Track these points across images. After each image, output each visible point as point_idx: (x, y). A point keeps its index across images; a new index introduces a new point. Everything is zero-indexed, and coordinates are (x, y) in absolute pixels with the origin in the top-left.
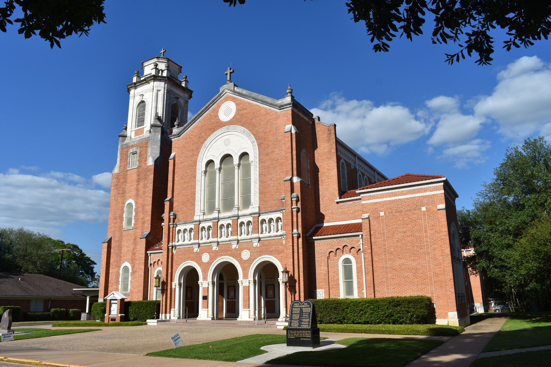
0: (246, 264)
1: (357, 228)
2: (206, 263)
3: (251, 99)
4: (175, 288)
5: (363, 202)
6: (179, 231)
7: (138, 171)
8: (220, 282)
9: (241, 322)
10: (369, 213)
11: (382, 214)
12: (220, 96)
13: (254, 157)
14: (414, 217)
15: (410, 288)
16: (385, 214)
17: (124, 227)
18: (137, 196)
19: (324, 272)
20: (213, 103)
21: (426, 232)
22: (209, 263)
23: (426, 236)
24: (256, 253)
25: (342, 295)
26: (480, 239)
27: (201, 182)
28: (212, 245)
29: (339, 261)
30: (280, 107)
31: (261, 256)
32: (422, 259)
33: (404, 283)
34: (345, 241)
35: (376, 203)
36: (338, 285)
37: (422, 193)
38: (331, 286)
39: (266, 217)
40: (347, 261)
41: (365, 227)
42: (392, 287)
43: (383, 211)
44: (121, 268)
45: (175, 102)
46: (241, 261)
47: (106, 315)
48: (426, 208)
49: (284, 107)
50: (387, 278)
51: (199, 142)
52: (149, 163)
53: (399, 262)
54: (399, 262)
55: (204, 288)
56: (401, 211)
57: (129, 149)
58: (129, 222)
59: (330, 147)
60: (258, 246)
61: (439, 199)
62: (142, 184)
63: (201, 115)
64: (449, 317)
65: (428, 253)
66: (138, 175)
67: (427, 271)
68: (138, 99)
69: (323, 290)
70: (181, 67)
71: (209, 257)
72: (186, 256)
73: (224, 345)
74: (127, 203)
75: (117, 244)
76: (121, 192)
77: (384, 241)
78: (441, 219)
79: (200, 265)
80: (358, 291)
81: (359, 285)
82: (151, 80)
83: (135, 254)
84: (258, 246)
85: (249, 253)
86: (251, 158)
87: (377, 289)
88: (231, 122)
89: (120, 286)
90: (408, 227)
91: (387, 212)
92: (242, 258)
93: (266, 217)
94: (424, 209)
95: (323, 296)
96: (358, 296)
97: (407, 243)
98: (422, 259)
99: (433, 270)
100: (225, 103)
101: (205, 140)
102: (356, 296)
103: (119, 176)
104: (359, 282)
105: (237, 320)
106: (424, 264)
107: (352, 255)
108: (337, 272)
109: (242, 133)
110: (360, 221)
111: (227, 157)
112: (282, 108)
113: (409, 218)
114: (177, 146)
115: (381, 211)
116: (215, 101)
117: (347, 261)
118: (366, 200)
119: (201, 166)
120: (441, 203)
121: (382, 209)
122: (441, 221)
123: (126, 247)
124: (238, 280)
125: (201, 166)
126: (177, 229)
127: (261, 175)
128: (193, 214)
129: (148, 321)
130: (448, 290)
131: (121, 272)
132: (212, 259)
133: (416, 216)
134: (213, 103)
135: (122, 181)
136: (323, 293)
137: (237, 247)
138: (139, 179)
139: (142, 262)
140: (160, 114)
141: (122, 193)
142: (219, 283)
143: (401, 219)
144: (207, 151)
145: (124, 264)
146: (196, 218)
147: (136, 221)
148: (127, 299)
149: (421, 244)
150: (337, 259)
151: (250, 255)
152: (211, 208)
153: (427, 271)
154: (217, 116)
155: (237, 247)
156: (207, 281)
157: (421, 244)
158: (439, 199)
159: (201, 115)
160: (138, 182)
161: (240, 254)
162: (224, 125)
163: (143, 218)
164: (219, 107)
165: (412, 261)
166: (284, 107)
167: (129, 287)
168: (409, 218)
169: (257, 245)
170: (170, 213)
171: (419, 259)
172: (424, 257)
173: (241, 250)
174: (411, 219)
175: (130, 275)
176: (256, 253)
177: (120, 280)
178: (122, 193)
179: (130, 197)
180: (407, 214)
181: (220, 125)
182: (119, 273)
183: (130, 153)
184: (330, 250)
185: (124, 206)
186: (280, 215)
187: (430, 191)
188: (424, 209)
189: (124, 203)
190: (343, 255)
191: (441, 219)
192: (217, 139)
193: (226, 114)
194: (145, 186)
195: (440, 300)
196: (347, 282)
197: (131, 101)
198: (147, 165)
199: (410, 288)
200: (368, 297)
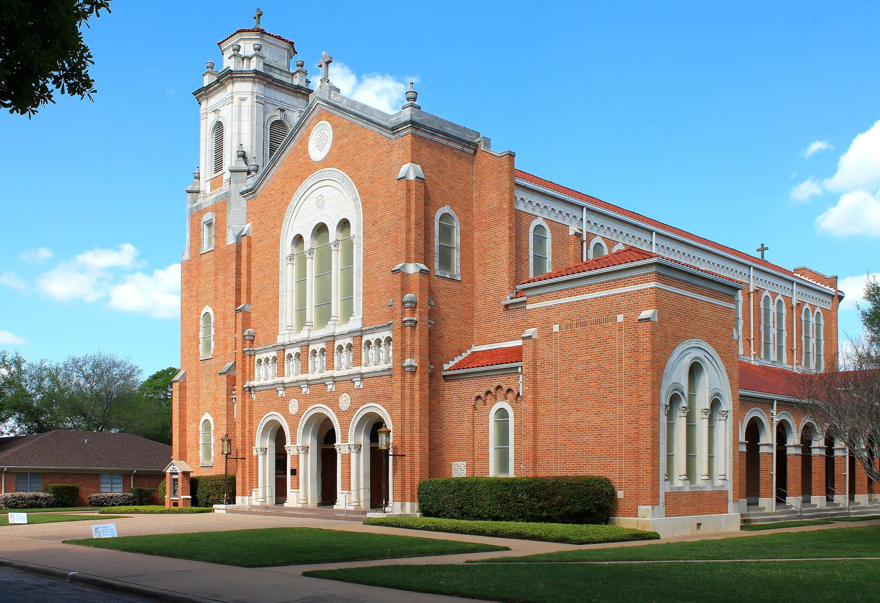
0: (293, 420)
1: (516, 354)
2: (294, 415)
3: (352, 116)
4: (257, 456)
5: (529, 307)
6: (260, 361)
7: (215, 256)
8: (323, 447)
9: (338, 511)
10: (536, 327)
11: (556, 328)
12: (309, 113)
13: (356, 230)
14: (605, 334)
15: (589, 462)
16: (560, 328)
17: (201, 355)
18: (215, 302)
19: (466, 432)
20: (300, 126)
21: (620, 361)
22: (298, 415)
23: (620, 369)
24: (359, 399)
25: (493, 472)
26: (85, 426)
27: (288, 274)
28: (301, 386)
29: (491, 410)
30: (392, 131)
31: (365, 404)
32: (610, 411)
33: (581, 453)
34: (501, 381)
35: (548, 309)
36: (487, 454)
37: (585, 295)
38: (477, 457)
39: (372, 337)
40: (502, 413)
41: (527, 353)
42: (562, 460)
43: (557, 324)
44: (201, 423)
45: (278, 118)
46: (287, 416)
47: (166, 497)
48: (624, 317)
49: (399, 130)
50: (556, 444)
51: (283, 203)
52: (229, 242)
53: (575, 416)
54: (575, 416)
55: (292, 457)
56: (584, 324)
57: (202, 216)
58: (208, 346)
59: (501, 198)
60: (361, 387)
61: (646, 300)
62: (220, 278)
63: (282, 151)
64: (639, 515)
65: (621, 401)
66: (216, 263)
67: (615, 434)
68: (212, 119)
69: (465, 463)
70: (292, 43)
71: (297, 406)
72: (268, 404)
73: (469, 546)
74: (203, 314)
75: (195, 383)
76: (194, 294)
77: (556, 378)
78: (642, 338)
79: (286, 418)
80: (515, 466)
81: (516, 455)
82: (227, 79)
83: (217, 400)
84: (361, 387)
85: (349, 399)
86: (353, 231)
87: (541, 463)
88: (326, 163)
89: (201, 452)
90: (594, 352)
91: (563, 326)
92: (340, 408)
93: (372, 337)
94: (620, 318)
95: (465, 473)
96: (515, 474)
97: (591, 383)
98: (610, 411)
99: (625, 431)
100: (317, 125)
101: (290, 198)
102: (511, 474)
103: (190, 265)
104: (516, 451)
105: (757, 504)
106: (613, 420)
107: (510, 404)
108: (487, 432)
109: (341, 183)
110: (519, 343)
111: (321, 229)
112: (396, 131)
113: (596, 336)
114: (253, 211)
115: (554, 324)
116: (303, 122)
117: (502, 413)
118: (533, 303)
119: (286, 247)
120: (648, 307)
121: (556, 319)
122: (642, 342)
123: (205, 389)
124: (285, 446)
125: (286, 247)
126: (257, 358)
127: (365, 260)
128: (276, 333)
129: (215, 506)
130: (641, 468)
131: (201, 429)
132: (302, 408)
133: (607, 332)
134: (300, 126)
135: (195, 273)
136: (465, 467)
137: (334, 390)
138: (217, 270)
139: (223, 412)
140: (247, 148)
141: (196, 296)
142: (322, 449)
143: (584, 337)
144: (293, 218)
145: (204, 416)
146: (280, 340)
147: (216, 344)
148: (193, 472)
149: (611, 385)
150: (488, 409)
151: (351, 403)
152: (302, 321)
153: (615, 434)
154: (306, 151)
155: (334, 390)
156: (347, 444)
157: (611, 385)
158: (646, 300)
159: (282, 151)
160: (216, 274)
161: (337, 401)
162: (316, 169)
163: (225, 339)
164: (309, 133)
165: (595, 414)
166: (399, 130)
167: (213, 455)
168: (596, 336)
169: (359, 386)
170: (243, 331)
171: (605, 411)
172: (614, 408)
173: (338, 394)
174: (599, 338)
175: (212, 435)
176: (359, 399)
177: (201, 442)
178: (196, 296)
179: (207, 302)
180: (593, 329)
181: (311, 167)
182: (198, 431)
183: (204, 223)
184: (477, 394)
185: (199, 318)
186: (387, 334)
187: (634, 285)
188: (620, 318)
189: (199, 314)
190: (496, 403)
191: (642, 338)
192: (307, 194)
193: (320, 148)
194: (225, 284)
195: (632, 485)
196: (499, 449)
197: (203, 123)
198: (227, 244)
199: (589, 462)
200: (523, 475)
